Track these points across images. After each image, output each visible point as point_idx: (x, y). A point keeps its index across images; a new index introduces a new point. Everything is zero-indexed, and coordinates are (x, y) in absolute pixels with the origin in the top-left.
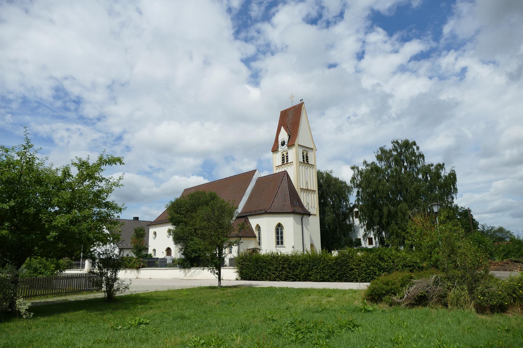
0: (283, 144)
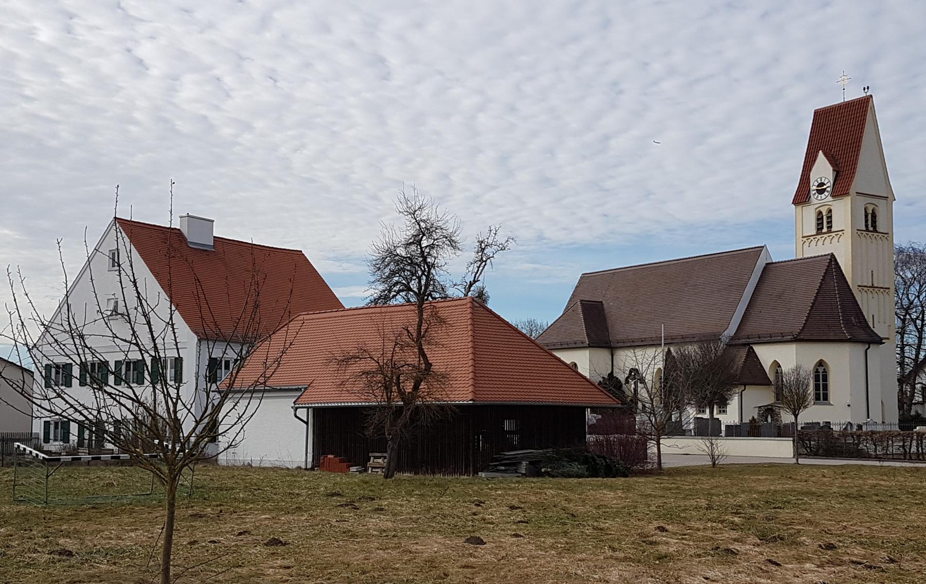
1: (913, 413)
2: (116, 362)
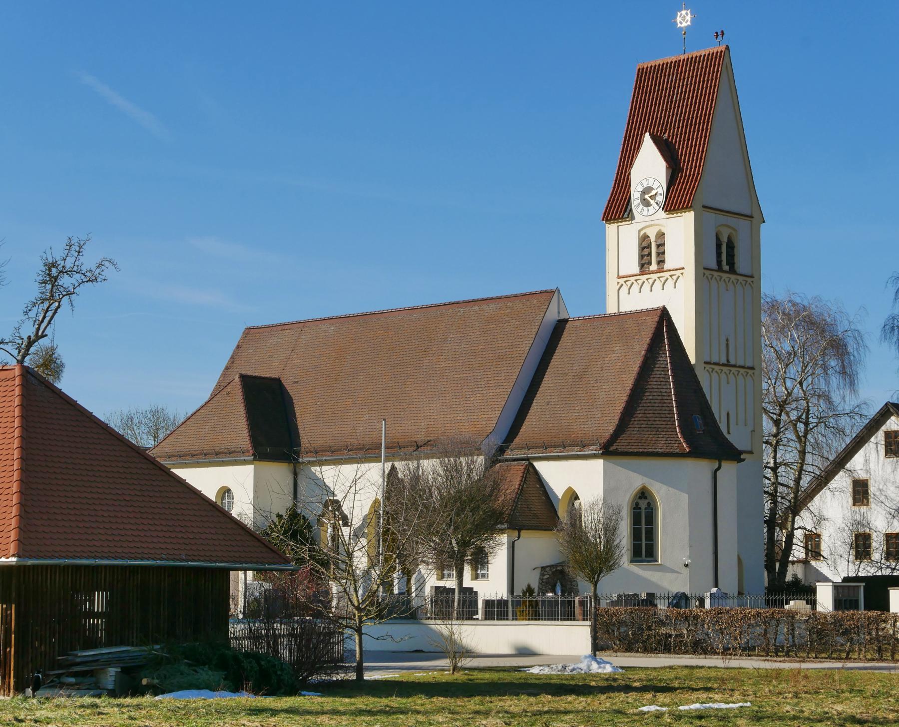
1: (789, 578)
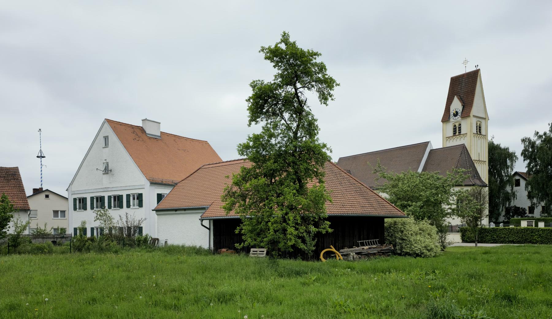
0: (456, 114)
2: (91, 197)
